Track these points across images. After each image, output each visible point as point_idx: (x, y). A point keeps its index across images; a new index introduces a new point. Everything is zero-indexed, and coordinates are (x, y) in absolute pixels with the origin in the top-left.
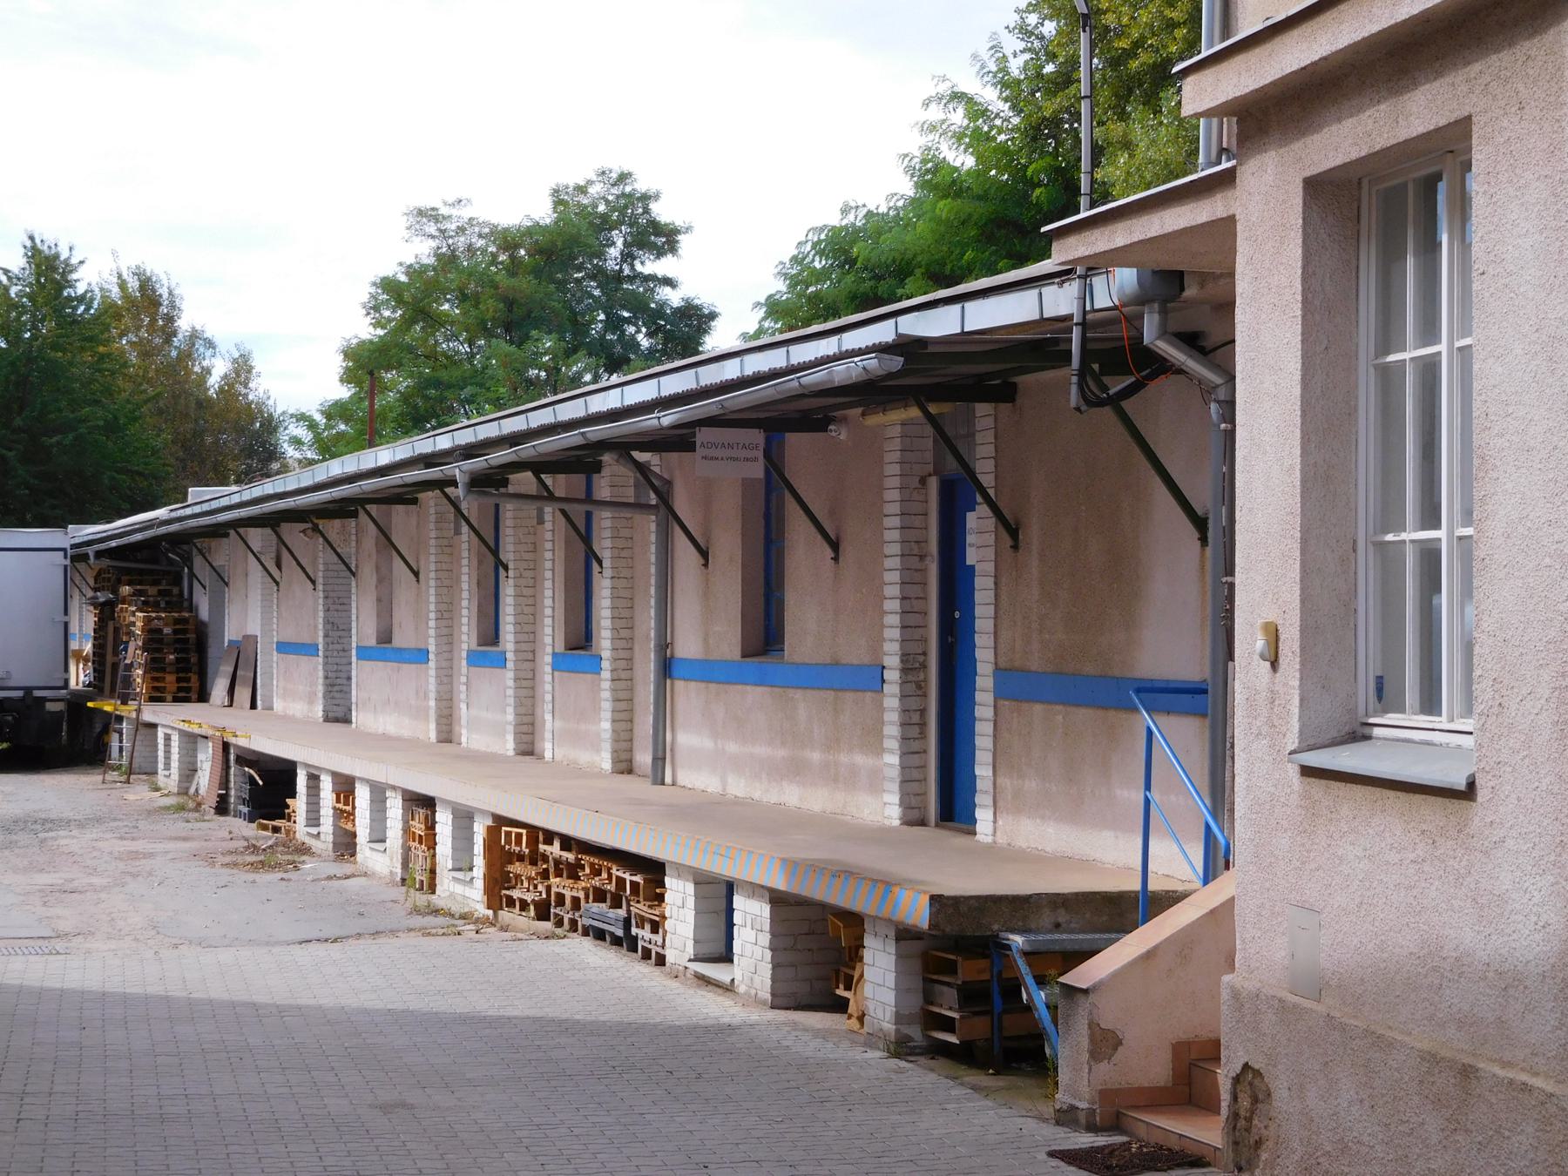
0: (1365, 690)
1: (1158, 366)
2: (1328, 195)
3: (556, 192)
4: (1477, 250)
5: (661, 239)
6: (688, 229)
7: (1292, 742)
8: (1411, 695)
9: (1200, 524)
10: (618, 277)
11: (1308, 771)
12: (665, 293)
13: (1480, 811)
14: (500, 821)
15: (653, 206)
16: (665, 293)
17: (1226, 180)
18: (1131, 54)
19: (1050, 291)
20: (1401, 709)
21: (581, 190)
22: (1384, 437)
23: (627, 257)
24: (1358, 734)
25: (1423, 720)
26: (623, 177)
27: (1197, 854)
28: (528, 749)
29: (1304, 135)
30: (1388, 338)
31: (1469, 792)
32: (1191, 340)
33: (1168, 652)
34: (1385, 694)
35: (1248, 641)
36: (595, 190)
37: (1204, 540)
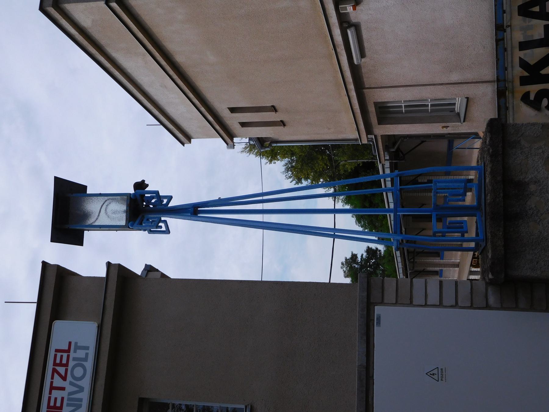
0: (452, 114)
1: (398, 149)
2: (381, 122)
3: (345, 277)
4: (392, 100)
5: (354, 256)
6: (352, 252)
7: (460, 124)
8: (453, 107)
9: (423, 142)
10: (361, 265)
11: (464, 121)
12: (364, 256)
13: (470, 96)
14: (472, 265)
15: (348, 258)
16: (364, 256)
17: (375, 136)
18: (327, 166)
19: (385, 166)
20: (455, 109)
21: (345, 272)
22: (416, 112)
23: (357, 263)
24: (458, 114)
25: (456, 105)
26: (342, 264)
27: (477, 140)
28: (457, 265)
29: (372, 125)
30: (401, 112)
31: (467, 98)
32: (394, 144)
33: (443, 146)
34: (453, 110)
35: (445, 131)
36: (345, 269)
37: (425, 141)
